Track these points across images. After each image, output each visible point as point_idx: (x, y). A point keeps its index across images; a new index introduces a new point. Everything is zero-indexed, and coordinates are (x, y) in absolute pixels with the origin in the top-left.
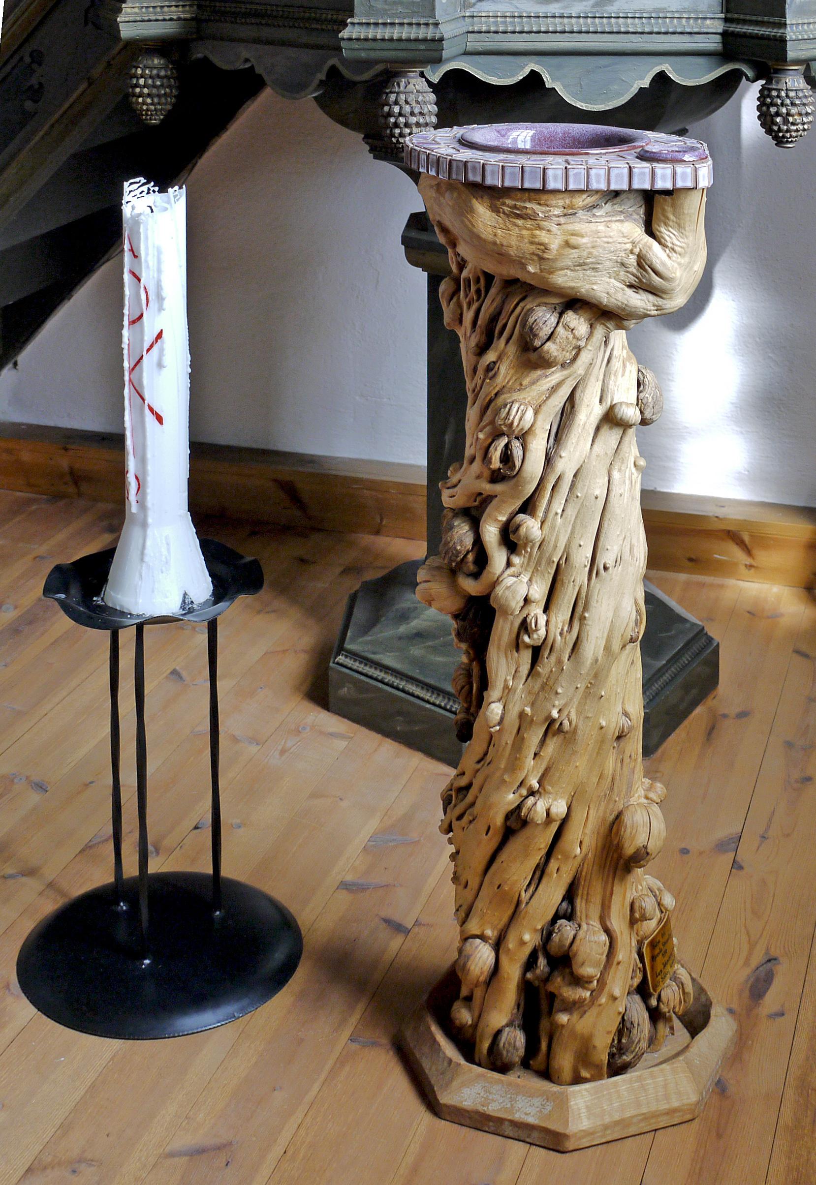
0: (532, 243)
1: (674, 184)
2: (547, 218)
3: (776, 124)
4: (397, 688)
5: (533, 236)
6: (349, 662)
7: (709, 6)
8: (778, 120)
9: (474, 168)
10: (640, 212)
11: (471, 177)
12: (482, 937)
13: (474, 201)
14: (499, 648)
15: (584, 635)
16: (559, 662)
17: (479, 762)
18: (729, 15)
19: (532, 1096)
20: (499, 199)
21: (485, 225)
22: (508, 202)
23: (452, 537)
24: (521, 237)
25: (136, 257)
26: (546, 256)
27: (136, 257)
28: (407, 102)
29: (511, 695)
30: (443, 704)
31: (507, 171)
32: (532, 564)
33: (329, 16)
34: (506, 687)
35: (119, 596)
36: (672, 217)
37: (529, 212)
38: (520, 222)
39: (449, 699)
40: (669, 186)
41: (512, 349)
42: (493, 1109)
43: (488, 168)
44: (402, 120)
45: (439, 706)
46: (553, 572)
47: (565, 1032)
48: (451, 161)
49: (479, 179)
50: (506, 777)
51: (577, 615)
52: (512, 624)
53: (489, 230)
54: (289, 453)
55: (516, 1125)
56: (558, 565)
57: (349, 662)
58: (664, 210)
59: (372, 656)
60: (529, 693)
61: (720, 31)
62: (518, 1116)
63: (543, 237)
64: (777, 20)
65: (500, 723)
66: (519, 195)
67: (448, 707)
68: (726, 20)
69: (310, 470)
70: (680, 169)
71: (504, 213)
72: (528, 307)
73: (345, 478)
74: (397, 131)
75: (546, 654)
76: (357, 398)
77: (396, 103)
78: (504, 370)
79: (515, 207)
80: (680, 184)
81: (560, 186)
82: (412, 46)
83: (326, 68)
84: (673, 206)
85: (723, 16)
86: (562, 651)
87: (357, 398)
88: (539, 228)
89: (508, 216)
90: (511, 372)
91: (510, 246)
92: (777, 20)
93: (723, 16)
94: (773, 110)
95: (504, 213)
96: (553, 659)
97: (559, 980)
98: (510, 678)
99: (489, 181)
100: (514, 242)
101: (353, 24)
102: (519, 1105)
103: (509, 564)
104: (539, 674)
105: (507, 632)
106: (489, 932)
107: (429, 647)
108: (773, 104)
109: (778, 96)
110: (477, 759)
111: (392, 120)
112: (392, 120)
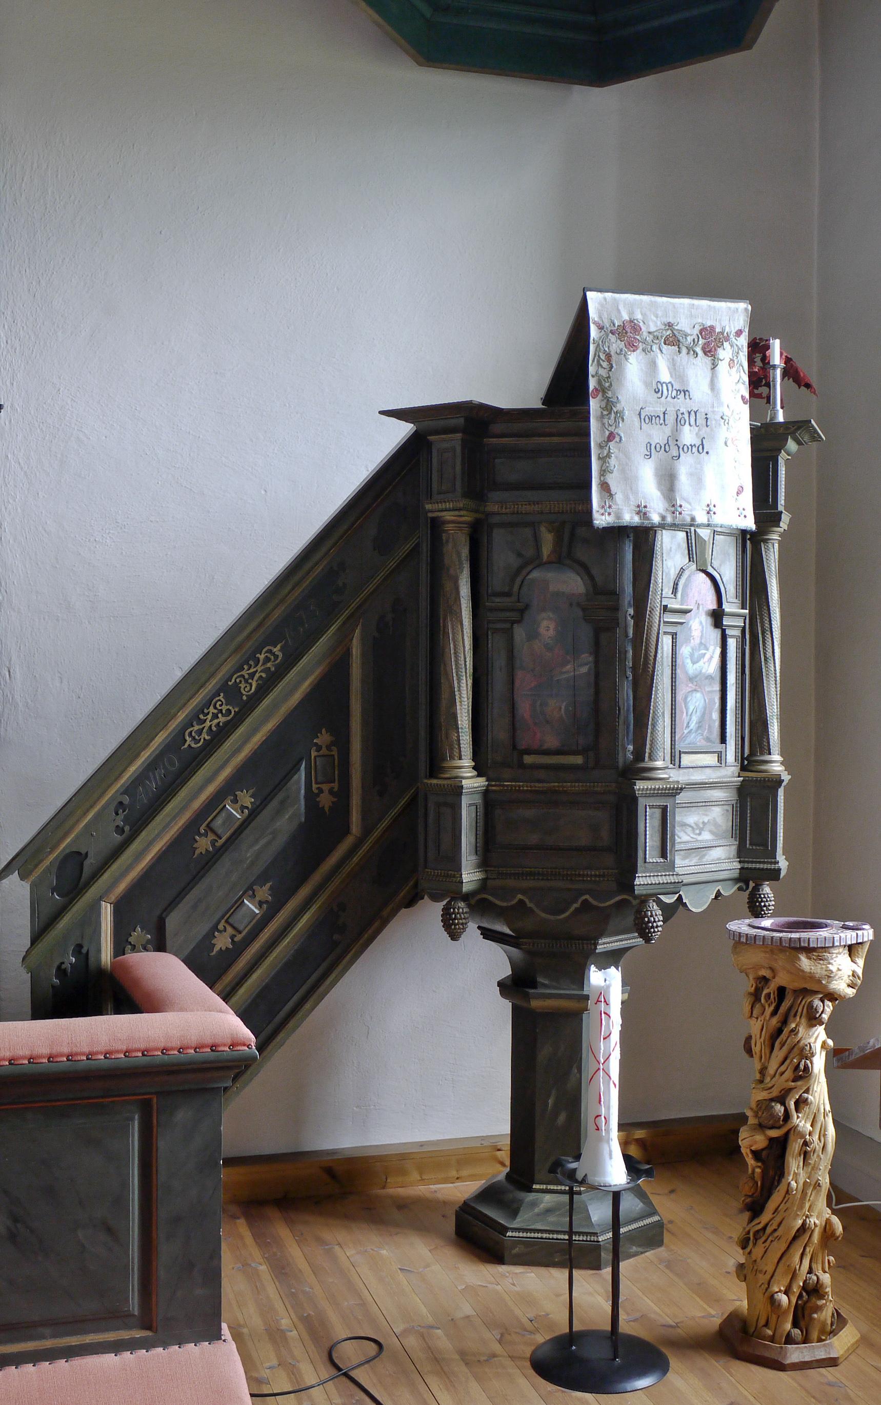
0: (826, 971)
1: (863, 939)
2: (832, 959)
3: (764, 911)
4: (549, 1239)
5: (828, 967)
6: (514, 1234)
7: (734, 856)
8: (765, 908)
9: (804, 941)
10: (846, 951)
11: (802, 944)
12: (780, 1291)
13: (799, 955)
14: (793, 1157)
15: (826, 1141)
16: (818, 1156)
17: (773, 1214)
18: (742, 859)
19: (820, 1348)
20: (810, 953)
21: (806, 965)
22: (814, 954)
23: (775, 1111)
24: (822, 968)
25: (607, 1004)
26: (832, 975)
27: (607, 1004)
28: (656, 915)
29: (798, 1176)
30: (585, 1239)
31: (819, 940)
32: (806, 1116)
33: (565, 872)
34: (795, 1173)
35: (603, 1179)
36: (860, 953)
37: (826, 957)
38: (821, 962)
39: (587, 1236)
40: (861, 941)
41: (804, 1021)
42: (807, 1359)
43: (811, 940)
44: (655, 924)
45: (583, 1241)
46: (813, 1117)
47: (816, 1322)
48: (809, 938)
49: (806, 945)
50: (798, 1213)
51: (822, 1135)
52: (799, 1144)
53: (808, 967)
54: (308, 1152)
55: (817, 1361)
56: (815, 1114)
57: (514, 1234)
58: (858, 951)
59: (528, 1227)
60: (807, 1173)
61: (739, 867)
62: (818, 1357)
63: (831, 967)
64: (773, 860)
65: (796, 1190)
66: (820, 950)
67: (588, 1239)
68: (740, 862)
69: (336, 1158)
70: (860, 932)
71: (813, 959)
72: (809, 1000)
73: (363, 1158)
74: (652, 930)
75: (812, 1154)
76: (355, 1108)
77: (652, 916)
78: (801, 1030)
79: (819, 956)
80: (864, 940)
81: (838, 944)
82: (667, 886)
83: (580, 901)
84: (862, 948)
85: (738, 860)
86: (819, 1151)
87: (355, 1108)
88: (829, 963)
89: (816, 960)
90: (804, 1030)
91: (817, 973)
92: (773, 860)
93: (738, 860)
94: (763, 904)
95: (813, 959)
96: (815, 1155)
97: (814, 1299)
98: (796, 1169)
99: (811, 945)
100: (819, 971)
101: (639, 877)
102: (817, 1353)
103: (798, 1117)
104: (810, 1164)
105: (797, 1148)
106: (782, 1288)
107: (559, 1214)
108: (762, 901)
109: (765, 897)
110: (772, 1212)
111: (650, 925)
112: (650, 925)
